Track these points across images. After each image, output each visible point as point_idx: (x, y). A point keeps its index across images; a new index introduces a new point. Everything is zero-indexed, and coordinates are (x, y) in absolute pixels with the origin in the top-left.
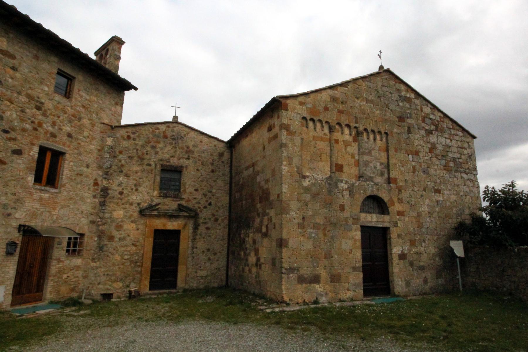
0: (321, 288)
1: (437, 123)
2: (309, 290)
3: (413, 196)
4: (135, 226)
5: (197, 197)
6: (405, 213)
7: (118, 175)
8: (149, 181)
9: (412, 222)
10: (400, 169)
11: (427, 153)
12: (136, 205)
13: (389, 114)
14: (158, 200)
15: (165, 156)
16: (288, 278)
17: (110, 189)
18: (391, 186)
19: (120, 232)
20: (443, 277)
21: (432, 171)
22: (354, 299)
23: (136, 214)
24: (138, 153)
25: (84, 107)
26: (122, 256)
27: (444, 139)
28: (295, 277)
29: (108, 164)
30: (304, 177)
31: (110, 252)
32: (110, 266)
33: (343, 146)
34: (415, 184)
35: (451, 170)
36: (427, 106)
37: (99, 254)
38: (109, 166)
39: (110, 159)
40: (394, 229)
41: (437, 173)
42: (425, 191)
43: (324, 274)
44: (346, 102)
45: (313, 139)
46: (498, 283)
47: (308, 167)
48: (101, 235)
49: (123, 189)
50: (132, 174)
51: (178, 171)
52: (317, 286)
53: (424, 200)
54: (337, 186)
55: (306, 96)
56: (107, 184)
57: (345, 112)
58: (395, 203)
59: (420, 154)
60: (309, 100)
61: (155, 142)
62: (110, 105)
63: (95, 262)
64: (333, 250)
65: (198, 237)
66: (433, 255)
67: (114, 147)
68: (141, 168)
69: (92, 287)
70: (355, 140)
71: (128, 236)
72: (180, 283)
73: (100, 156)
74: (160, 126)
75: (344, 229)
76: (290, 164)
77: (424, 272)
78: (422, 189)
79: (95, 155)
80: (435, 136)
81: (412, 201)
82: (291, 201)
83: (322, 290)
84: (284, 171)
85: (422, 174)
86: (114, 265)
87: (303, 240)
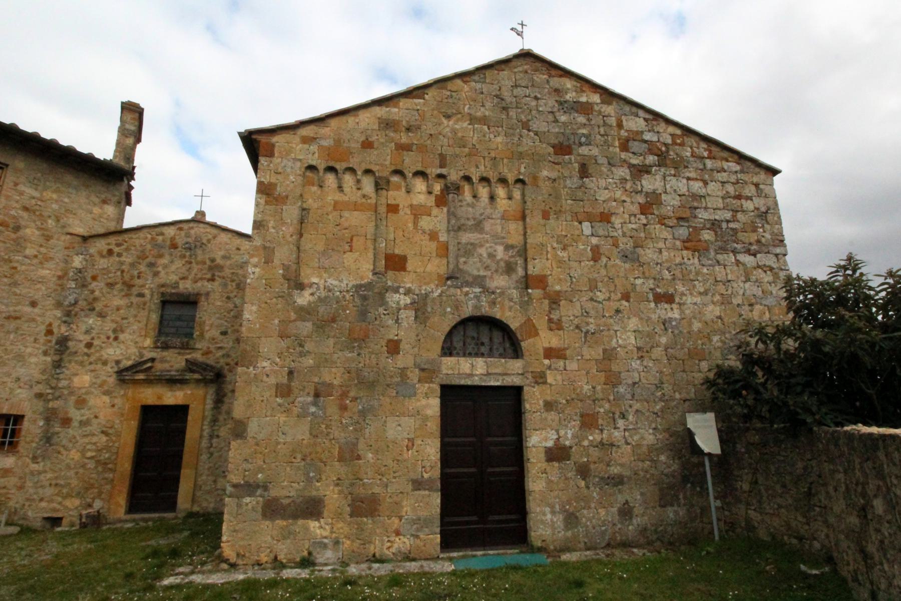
0: (325, 529)
1: (664, 149)
2: (290, 533)
3: (592, 313)
4: (108, 401)
5: (225, 346)
6: (568, 352)
7: (86, 316)
8: (139, 322)
9: (588, 373)
10: (557, 255)
11: (635, 216)
12: (113, 364)
13: (528, 142)
15: (170, 278)
16: (239, 506)
17: (70, 340)
18: (528, 294)
19: (83, 411)
20: (682, 501)
22: (412, 556)
23: (112, 380)
24: (123, 276)
25: (26, 209)
26: (83, 452)
27: (685, 181)
28: (257, 503)
29: (71, 299)
30: (301, 287)
31: (63, 446)
32: (61, 470)
34: (600, 284)
35: (707, 249)
36: (637, 116)
37: (44, 448)
38: (73, 302)
39: (75, 290)
40: (537, 390)
41: (664, 258)
42: (628, 301)
44: (419, 128)
46: (800, 526)
47: (317, 265)
48: (50, 416)
49: (93, 339)
50: (110, 313)
51: (190, 302)
52: (313, 525)
53: (626, 320)
54: (382, 301)
55: (317, 124)
57: (414, 147)
58: (540, 332)
59: (613, 219)
60: (324, 131)
61: (153, 256)
62: (89, 204)
63: (37, 463)
65: (221, 418)
66: (651, 449)
67: (84, 270)
68: (127, 301)
69: (29, 506)
70: (441, 201)
71: (96, 417)
72: (183, 502)
73: (60, 285)
74: (166, 230)
75: (394, 394)
76: (266, 262)
77: (620, 491)
78: (619, 295)
81: (588, 324)
82: (263, 339)
83: (325, 534)
84: (252, 276)
85: (618, 262)
86: (68, 467)
87: (285, 422)
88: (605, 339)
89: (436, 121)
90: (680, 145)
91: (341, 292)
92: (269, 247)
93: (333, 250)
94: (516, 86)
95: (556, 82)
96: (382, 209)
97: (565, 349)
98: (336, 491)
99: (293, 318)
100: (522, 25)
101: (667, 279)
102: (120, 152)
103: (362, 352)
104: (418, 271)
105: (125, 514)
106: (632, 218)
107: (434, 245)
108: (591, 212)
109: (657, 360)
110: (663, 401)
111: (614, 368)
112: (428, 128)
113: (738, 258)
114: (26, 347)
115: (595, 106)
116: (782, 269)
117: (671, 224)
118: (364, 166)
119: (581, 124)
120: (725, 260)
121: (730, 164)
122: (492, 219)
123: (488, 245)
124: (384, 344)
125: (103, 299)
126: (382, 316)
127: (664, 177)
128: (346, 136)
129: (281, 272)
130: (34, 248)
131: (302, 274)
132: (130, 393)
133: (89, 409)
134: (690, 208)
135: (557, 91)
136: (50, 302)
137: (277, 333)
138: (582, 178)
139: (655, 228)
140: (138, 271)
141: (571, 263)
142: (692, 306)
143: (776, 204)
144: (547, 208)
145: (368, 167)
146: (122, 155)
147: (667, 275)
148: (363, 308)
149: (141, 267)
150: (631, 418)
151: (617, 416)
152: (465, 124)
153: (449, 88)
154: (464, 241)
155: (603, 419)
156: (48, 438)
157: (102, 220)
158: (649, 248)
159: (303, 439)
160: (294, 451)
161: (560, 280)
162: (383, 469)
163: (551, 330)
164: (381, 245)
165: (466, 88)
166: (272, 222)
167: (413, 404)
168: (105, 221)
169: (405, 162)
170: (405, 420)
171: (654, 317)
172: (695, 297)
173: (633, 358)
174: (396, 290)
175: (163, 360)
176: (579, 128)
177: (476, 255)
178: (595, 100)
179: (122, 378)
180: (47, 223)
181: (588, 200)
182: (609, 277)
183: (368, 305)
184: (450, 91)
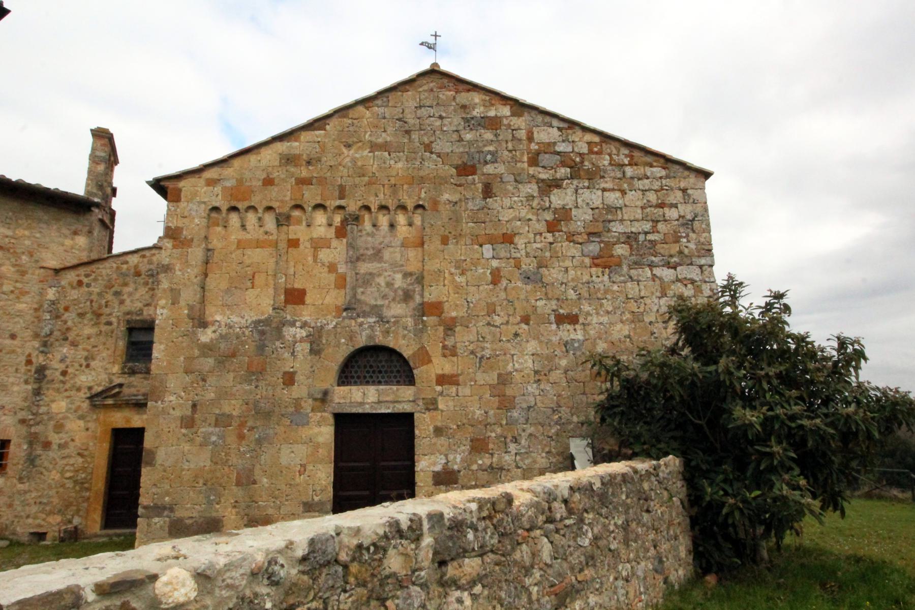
1: (578, 159)
3: (489, 337)
6: (461, 378)
7: (61, 346)
8: (108, 349)
9: (481, 398)
10: (454, 281)
11: (541, 234)
12: (86, 391)
13: (431, 165)
14: (121, 379)
15: (135, 305)
16: (149, 525)
18: (423, 321)
19: (61, 435)
21: (553, 274)
23: (86, 405)
24: (92, 306)
26: (62, 472)
27: (599, 193)
28: (165, 522)
29: (47, 330)
30: (204, 324)
31: (45, 468)
32: (43, 489)
33: (309, 252)
34: (498, 309)
35: (619, 265)
36: (551, 126)
37: (29, 469)
38: (48, 333)
39: (50, 322)
40: (427, 416)
41: (570, 278)
42: (527, 324)
43: (233, 517)
45: (238, 247)
47: (221, 303)
48: (33, 440)
49: (67, 367)
50: (81, 341)
53: (524, 344)
54: (280, 336)
55: (223, 165)
56: (44, 360)
57: (314, 181)
58: (434, 360)
59: (516, 239)
60: (228, 172)
61: (119, 286)
64: (258, 466)
69: (18, 522)
70: (341, 233)
71: (73, 440)
75: (288, 423)
76: (173, 304)
78: (519, 318)
79: (28, 317)
80: (570, 191)
81: (483, 349)
84: (160, 317)
85: (519, 284)
86: (50, 487)
88: (501, 364)
89: (336, 151)
90: (597, 153)
91: (240, 328)
92: (175, 289)
93: (236, 287)
94: (420, 107)
95: (464, 97)
96: (283, 245)
97: (458, 375)
98: (234, 513)
99: (196, 355)
100: (436, 36)
101: (571, 299)
102: (91, 180)
103: (260, 384)
104: (317, 303)
105: (101, 530)
106: (538, 237)
107: (332, 277)
108: (492, 234)
109: (555, 383)
110: (560, 425)
111: (509, 392)
112: (328, 160)
113: (654, 272)
114: (8, 377)
115: (504, 120)
116: (705, 282)
117: (580, 241)
118: (266, 204)
119: (487, 140)
120: (639, 275)
121: (654, 169)
122: (392, 247)
123: (386, 274)
124: (280, 376)
125: (74, 328)
126: (279, 350)
127: (577, 191)
128: (248, 175)
129: (186, 312)
130: (10, 284)
131: (207, 312)
132: (101, 417)
133: (67, 433)
134: (603, 221)
135: (464, 107)
136: (29, 333)
137: (182, 370)
138: (485, 198)
139: (562, 246)
140: (105, 301)
141: (469, 288)
142: (597, 325)
143: (706, 210)
144: (447, 233)
145: (270, 205)
146: (95, 183)
147: (572, 294)
148: (262, 342)
149: (108, 296)
150: (523, 442)
151: (508, 440)
152: (366, 153)
153: (350, 117)
154: (362, 271)
155: (494, 444)
156: (31, 460)
157: (74, 251)
158: (554, 268)
159: (205, 466)
160: (196, 476)
161: (457, 306)
162: (277, 492)
163: (444, 356)
164: (280, 281)
165: (368, 114)
166: (178, 265)
167: (305, 432)
168: (77, 252)
169: (305, 196)
170: (297, 447)
171: (555, 339)
172: (602, 316)
173: (529, 382)
174: (293, 324)
175: (130, 386)
176: (485, 146)
177: (373, 285)
178: (504, 113)
179: (94, 403)
180: (21, 259)
181: (491, 221)
182: (509, 300)
183: (265, 339)
184: (352, 118)
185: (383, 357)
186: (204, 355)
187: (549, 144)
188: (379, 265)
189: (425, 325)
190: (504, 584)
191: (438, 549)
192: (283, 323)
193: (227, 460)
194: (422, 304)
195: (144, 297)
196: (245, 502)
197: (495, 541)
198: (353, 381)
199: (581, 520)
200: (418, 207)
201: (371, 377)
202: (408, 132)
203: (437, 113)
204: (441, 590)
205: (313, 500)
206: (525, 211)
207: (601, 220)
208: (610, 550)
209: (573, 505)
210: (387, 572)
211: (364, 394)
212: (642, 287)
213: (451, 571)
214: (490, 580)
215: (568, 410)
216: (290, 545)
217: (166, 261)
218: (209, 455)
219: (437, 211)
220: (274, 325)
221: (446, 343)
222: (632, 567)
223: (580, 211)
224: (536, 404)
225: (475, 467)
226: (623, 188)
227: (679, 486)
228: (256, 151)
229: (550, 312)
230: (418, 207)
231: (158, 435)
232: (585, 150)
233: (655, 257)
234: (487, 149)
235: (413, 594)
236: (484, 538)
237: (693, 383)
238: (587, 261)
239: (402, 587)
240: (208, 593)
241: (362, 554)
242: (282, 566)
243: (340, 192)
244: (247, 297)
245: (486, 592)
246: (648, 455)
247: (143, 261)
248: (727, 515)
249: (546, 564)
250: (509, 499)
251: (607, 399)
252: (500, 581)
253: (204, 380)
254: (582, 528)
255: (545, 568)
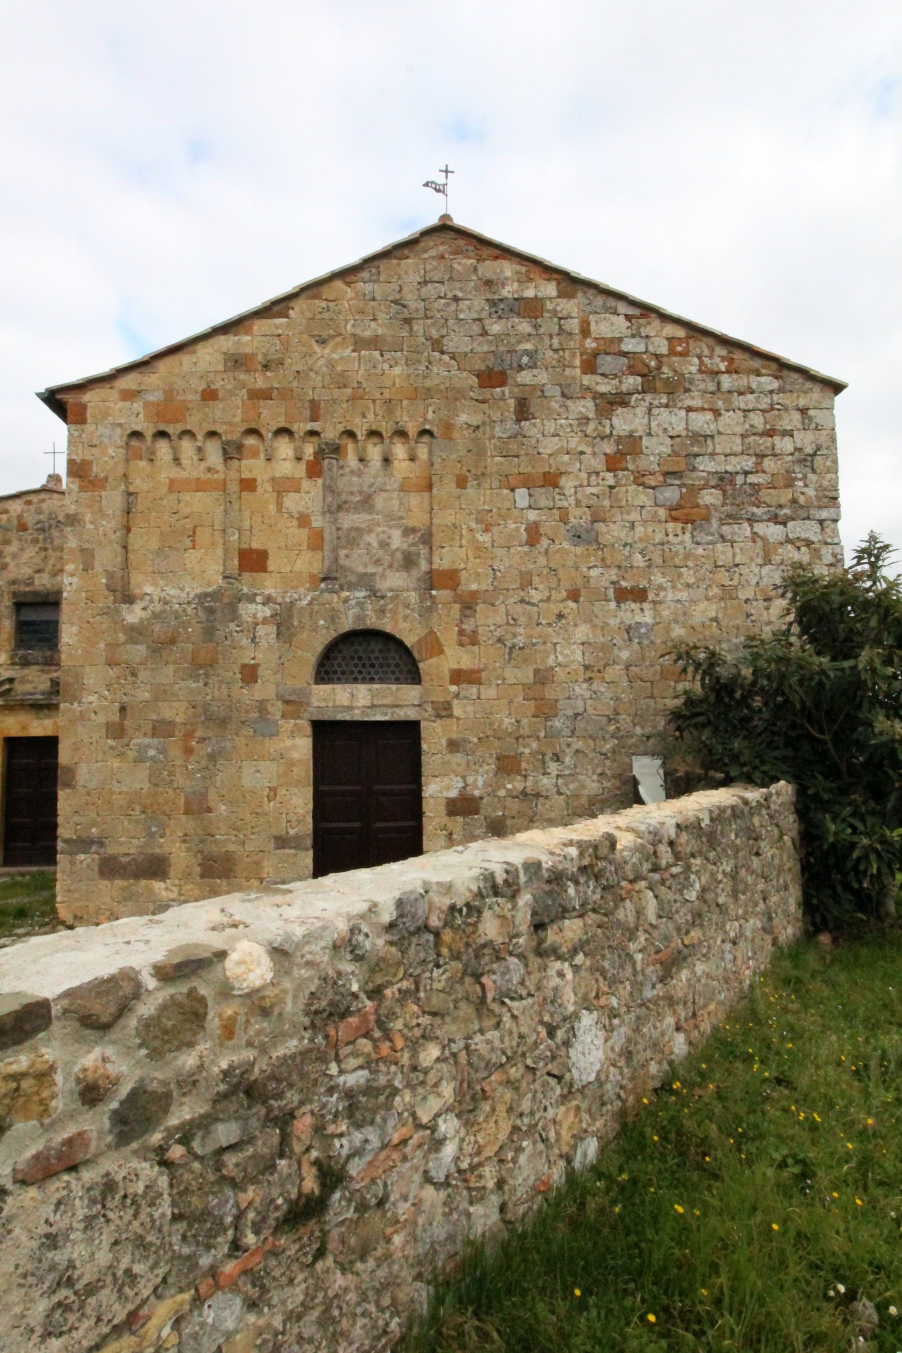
3: (522, 620)
6: (484, 675)
9: (510, 702)
10: (474, 540)
11: (597, 473)
16: (72, 863)
18: (431, 596)
27: (683, 413)
28: (93, 860)
30: (130, 599)
33: (270, 497)
34: (536, 579)
35: (707, 519)
36: (615, 313)
40: (438, 725)
41: (637, 536)
42: (576, 601)
47: (151, 569)
53: (571, 629)
54: (234, 615)
55: (143, 369)
57: (275, 393)
58: (447, 650)
59: (563, 481)
60: (152, 380)
70: (314, 470)
75: (251, 733)
76: (85, 570)
78: (564, 594)
80: (641, 411)
81: (515, 635)
84: (69, 588)
85: (566, 545)
89: (304, 349)
90: (681, 354)
94: (426, 282)
95: (490, 268)
96: (233, 487)
97: (479, 671)
100: (447, 172)
106: (593, 478)
107: (304, 534)
109: (612, 682)
110: (617, 738)
111: (550, 694)
112: (294, 362)
113: (755, 530)
115: (548, 302)
116: (826, 543)
117: (653, 484)
120: (733, 533)
121: (763, 379)
123: (379, 529)
124: (237, 670)
126: (235, 634)
127: (650, 410)
128: (180, 384)
131: (133, 582)
135: (489, 283)
138: (518, 421)
139: (627, 491)
143: (833, 440)
147: (638, 560)
150: (567, 760)
151: (547, 758)
152: (347, 352)
160: (131, 801)
161: (478, 575)
163: (461, 645)
167: (274, 746)
169: (262, 416)
170: (263, 765)
172: (680, 591)
174: (251, 599)
175: (24, 681)
176: (519, 342)
181: (527, 455)
184: (326, 300)
185: (376, 646)
186: (133, 641)
187: (612, 340)
188: (370, 517)
189: (434, 603)
190: (607, 951)
191: (537, 909)
192: (240, 598)
193: (171, 782)
194: (430, 572)
195: (34, 561)
196: (197, 835)
197: (597, 897)
198: (335, 677)
199: (688, 868)
200: (424, 432)
201: (360, 672)
202: (408, 321)
203: (451, 291)
204: (540, 961)
205: (287, 833)
206: (576, 439)
207: (684, 453)
208: (718, 905)
209: (680, 849)
210: (481, 941)
211: (353, 695)
212: (738, 551)
213: (551, 936)
214: (591, 946)
215: (629, 719)
216: (373, 908)
217: (72, 509)
218: (147, 773)
219: (451, 439)
220: (225, 601)
221: (464, 627)
222: (740, 926)
223: (654, 440)
224: (585, 710)
225: (502, 793)
226: (716, 407)
227: (790, 821)
228: (191, 349)
229: (608, 584)
230: (424, 432)
231: (76, 748)
232: (664, 350)
233: (758, 507)
234: (522, 347)
235: (512, 967)
236: (586, 893)
237: (820, 684)
238: (662, 513)
239: (499, 959)
240: (286, 973)
241: (454, 918)
242: (367, 935)
243: (312, 410)
244: (187, 562)
245: (588, 963)
246: (749, 780)
247: (29, 510)
248: (859, 859)
249: (651, 924)
250: (612, 841)
251: (685, 704)
252: (603, 948)
253: (134, 675)
254: (689, 877)
255: (650, 930)
